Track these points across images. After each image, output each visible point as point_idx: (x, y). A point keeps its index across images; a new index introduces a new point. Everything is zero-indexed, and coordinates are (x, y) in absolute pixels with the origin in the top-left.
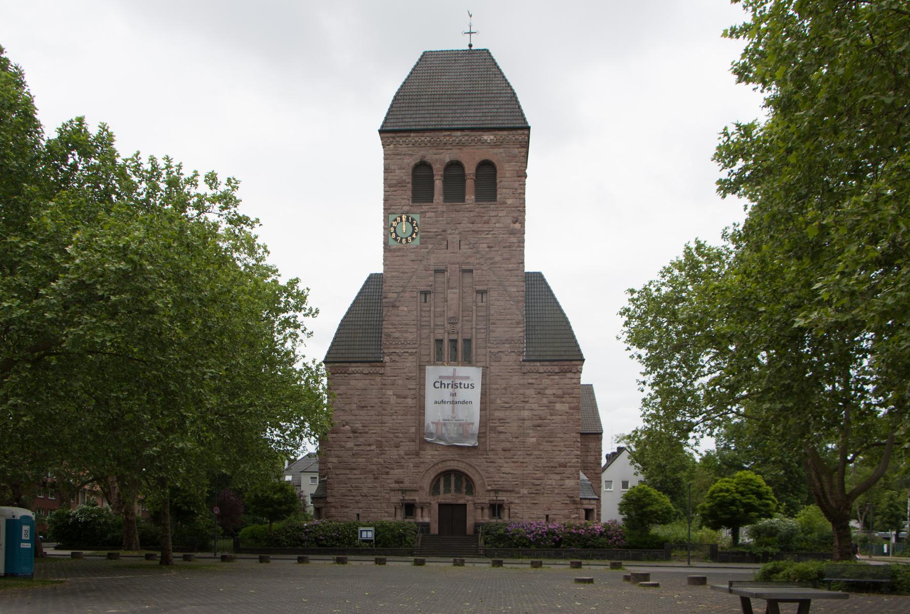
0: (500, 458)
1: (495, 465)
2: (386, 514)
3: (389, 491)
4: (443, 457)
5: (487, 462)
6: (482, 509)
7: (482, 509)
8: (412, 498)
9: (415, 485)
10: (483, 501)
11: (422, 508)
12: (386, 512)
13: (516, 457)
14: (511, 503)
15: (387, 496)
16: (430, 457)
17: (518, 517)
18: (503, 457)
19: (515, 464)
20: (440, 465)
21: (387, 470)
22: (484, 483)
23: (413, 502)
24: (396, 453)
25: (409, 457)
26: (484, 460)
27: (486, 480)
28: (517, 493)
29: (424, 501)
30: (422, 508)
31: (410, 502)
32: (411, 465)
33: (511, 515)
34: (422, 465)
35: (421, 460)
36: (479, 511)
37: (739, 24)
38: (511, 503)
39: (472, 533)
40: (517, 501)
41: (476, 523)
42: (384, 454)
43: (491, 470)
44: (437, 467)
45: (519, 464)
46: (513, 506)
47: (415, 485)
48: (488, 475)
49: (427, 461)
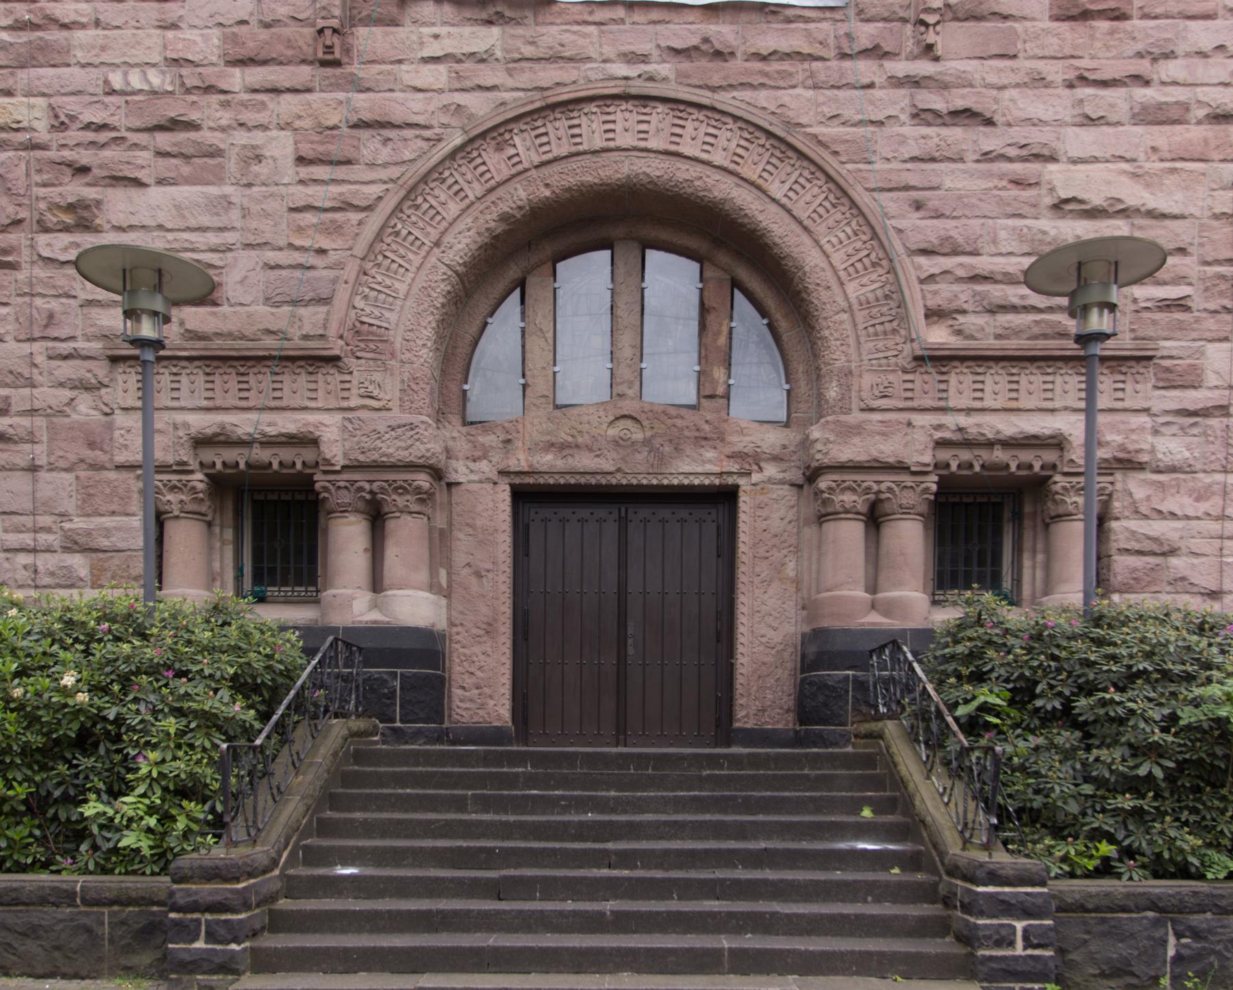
0: (1039, 81)
1: (991, 141)
2: (79, 564)
3: (101, 370)
4: (548, 75)
5: (921, 116)
6: (875, 518)
7: (875, 518)
8: (287, 424)
9: (311, 317)
10: (888, 450)
11: (377, 517)
12: (73, 545)
13: (1171, 69)
14: (1128, 464)
15: (85, 409)
16: (437, 76)
17: (1181, 583)
18: (1056, 72)
19: (1161, 136)
20: (523, 146)
21: (75, 190)
22: (894, 296)
23: (298, 457)
24: (152, 45)
25: (257, 76)
26: (898, 102)
27: (913, 268)
28: (1171, 381)
29: (392, 449)
30: (377, 517)
31: (1012, 460)
32: (281, 147)
33: (1122, 565)
34: (371, 146)
35: (364, 104)
36: (851, 533)
37: (518, 309)
38: (1128, 464)
39: (781, 720)
40: (1171, 447)
41: (806, 639)
42: (57, 57)
43: (954, 179)
44: (495, 162)
45: (1193, 134)
46: (1136, 486)
47: (311, 317)
48: (929, 230)
49: (413, 107)
